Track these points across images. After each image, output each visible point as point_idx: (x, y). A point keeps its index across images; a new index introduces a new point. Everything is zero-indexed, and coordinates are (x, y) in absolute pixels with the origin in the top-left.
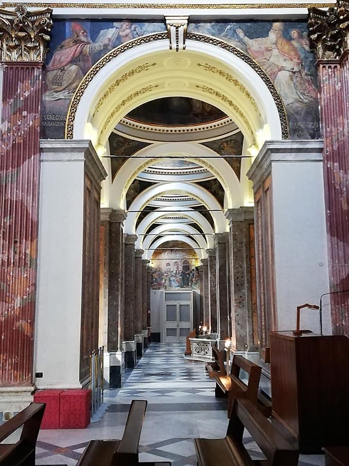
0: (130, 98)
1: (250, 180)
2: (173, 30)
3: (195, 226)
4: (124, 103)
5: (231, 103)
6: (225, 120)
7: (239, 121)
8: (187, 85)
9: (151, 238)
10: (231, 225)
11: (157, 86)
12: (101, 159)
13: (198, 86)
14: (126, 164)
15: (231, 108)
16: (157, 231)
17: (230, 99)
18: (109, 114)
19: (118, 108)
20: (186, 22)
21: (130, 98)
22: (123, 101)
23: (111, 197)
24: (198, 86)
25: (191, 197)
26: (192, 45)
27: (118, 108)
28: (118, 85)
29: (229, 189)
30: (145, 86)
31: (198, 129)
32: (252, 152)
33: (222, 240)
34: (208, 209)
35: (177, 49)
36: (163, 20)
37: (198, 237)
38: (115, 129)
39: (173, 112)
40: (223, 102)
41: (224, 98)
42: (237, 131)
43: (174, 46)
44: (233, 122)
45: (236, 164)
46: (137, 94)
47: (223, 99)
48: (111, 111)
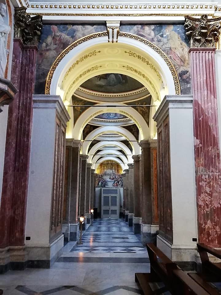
0: (85, 73)
1: (155, 122)
2: (110, 31)
3: (121, 151)
4: (81, 76)
5: (144, 76)
6: (143, 88)
7: (151, 90)
8: (118, 66)
9: (97, 157)
10: (143, 150)
11: (101, 66)
12: (67, 108)
13: (124, 66)
14: (90, 109)
15: (144, 79)
16: (100, 153)
17: (143, 73)
18: (72, 83)
19: (77, 79)
20: (119, 25)
21: (85, 73)
22: (80, 75)
23: (73, 133)
24: (124, 66)
25: (120, 135)
26: (121, 40)
27: (77, 79)
28: (78, 64)
29: (141, 129)
30: (94, 66)
31: (140, 91)
32: (156, 104)
33: (136, 159)
34: (128, 140)
35: (113, 42)
36: (104, 24)
37: (123, 157)
38: (74, 93)
39: (116, 84)
40: (139, 76)
41: (140, 73)
42: (149, 95)
43: (111, 40)
44: (147, 90)
45: (145, 114)
46: (89, 71)
47: (139, 74)
48: (73, 80)
